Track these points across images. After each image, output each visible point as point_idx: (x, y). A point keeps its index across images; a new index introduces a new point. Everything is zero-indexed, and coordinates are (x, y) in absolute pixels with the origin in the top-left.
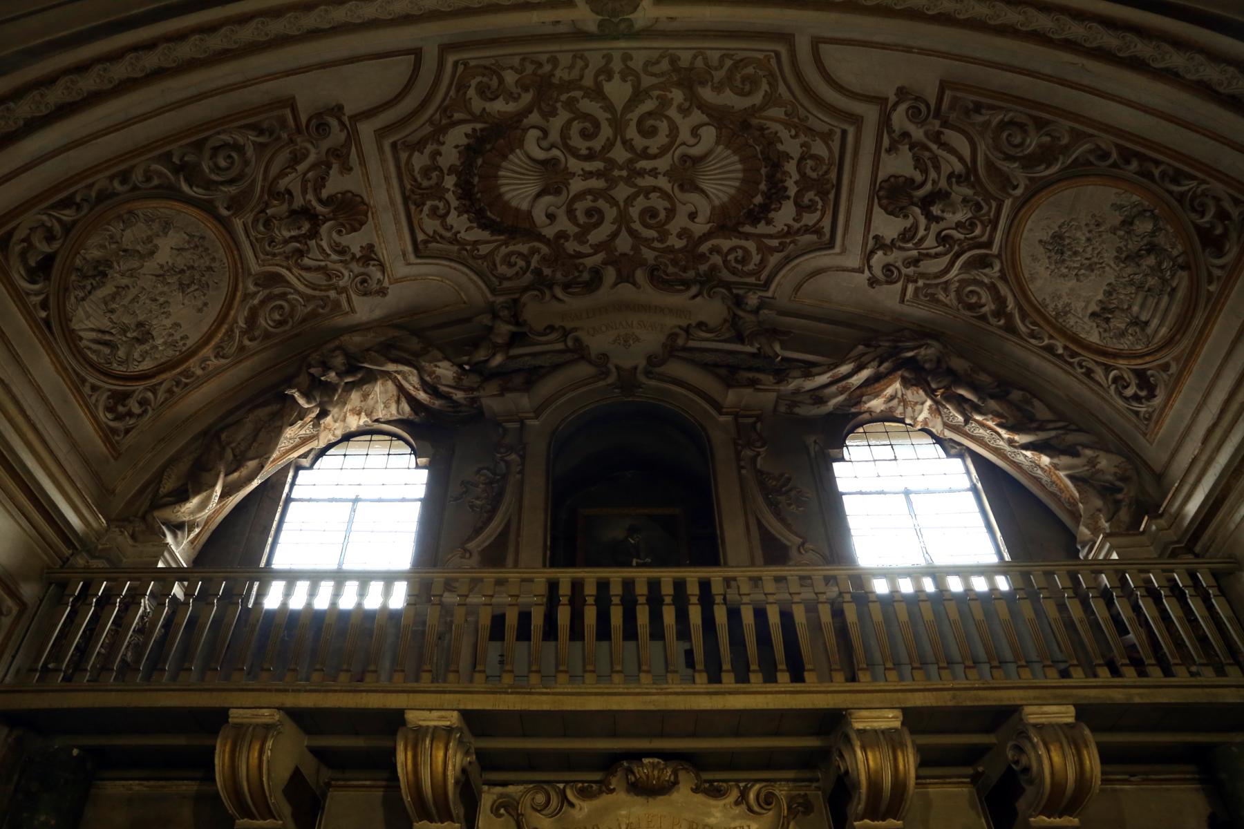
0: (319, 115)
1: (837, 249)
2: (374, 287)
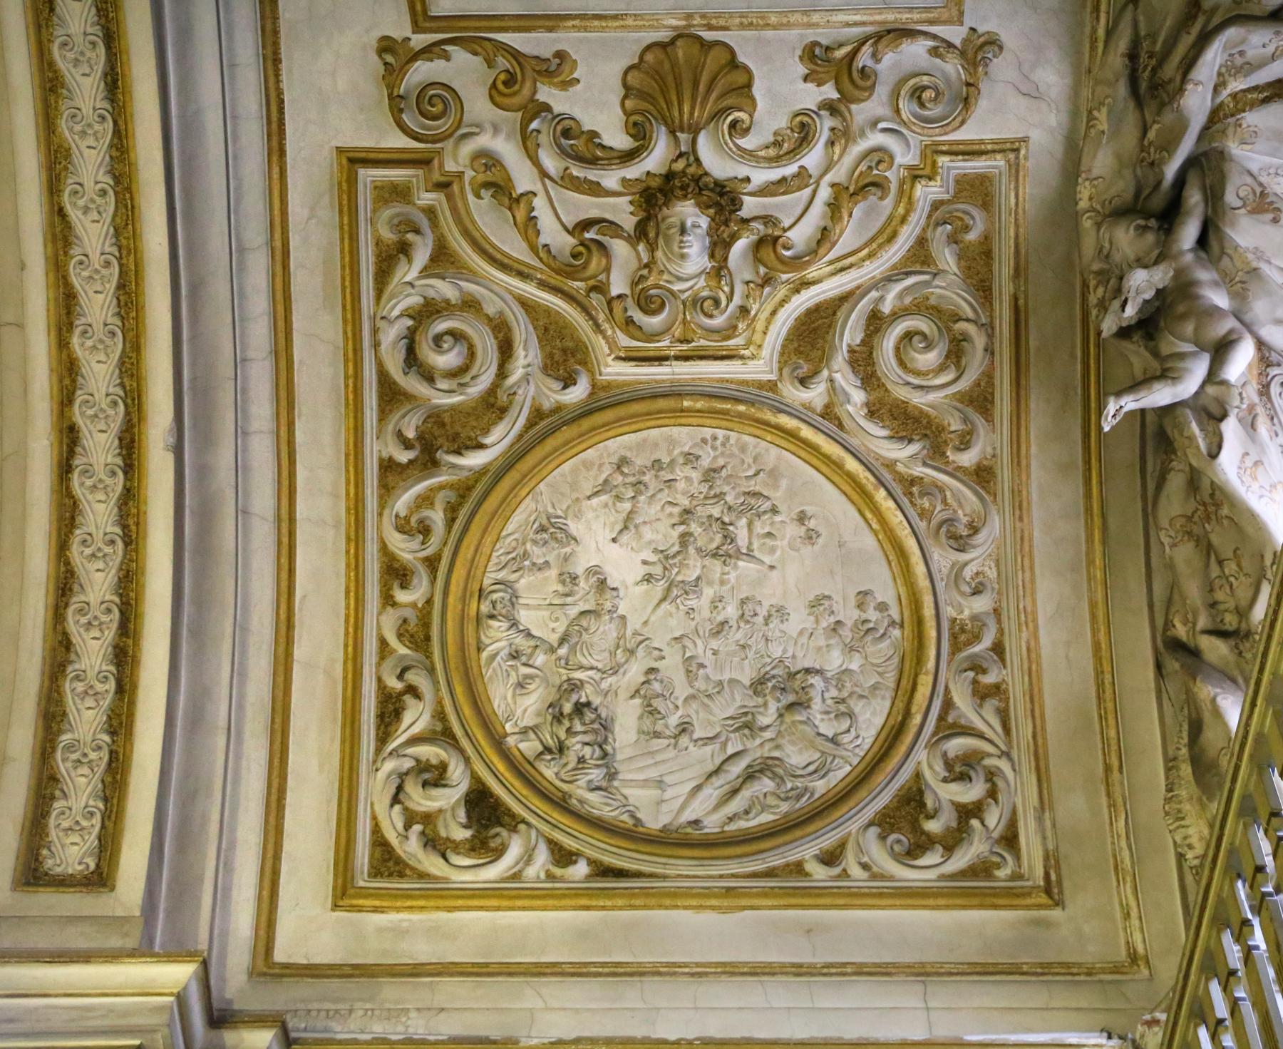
0: (396, 104)
2: (952, 67)
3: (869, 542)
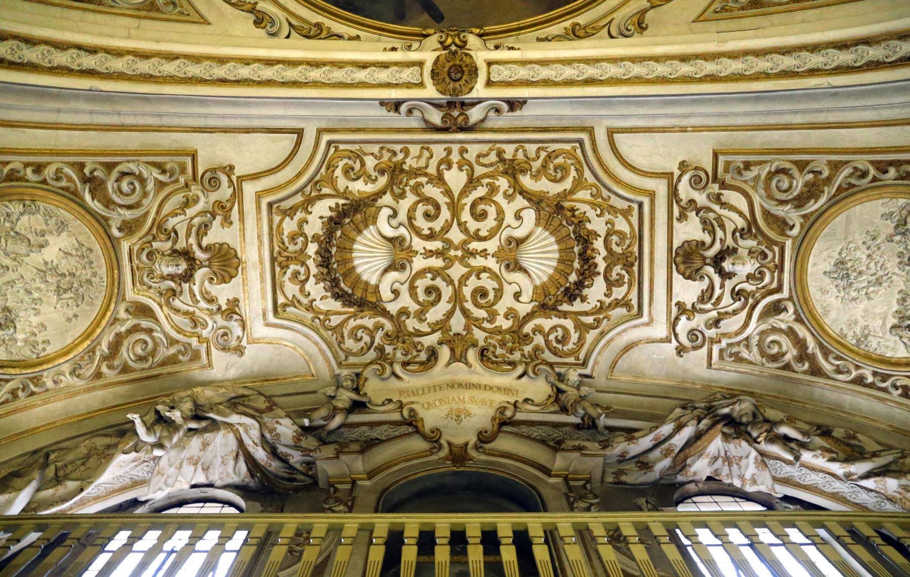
0: (214, 170)
1: (645, 318)
2: (234, 343)
3: (69, 341)
